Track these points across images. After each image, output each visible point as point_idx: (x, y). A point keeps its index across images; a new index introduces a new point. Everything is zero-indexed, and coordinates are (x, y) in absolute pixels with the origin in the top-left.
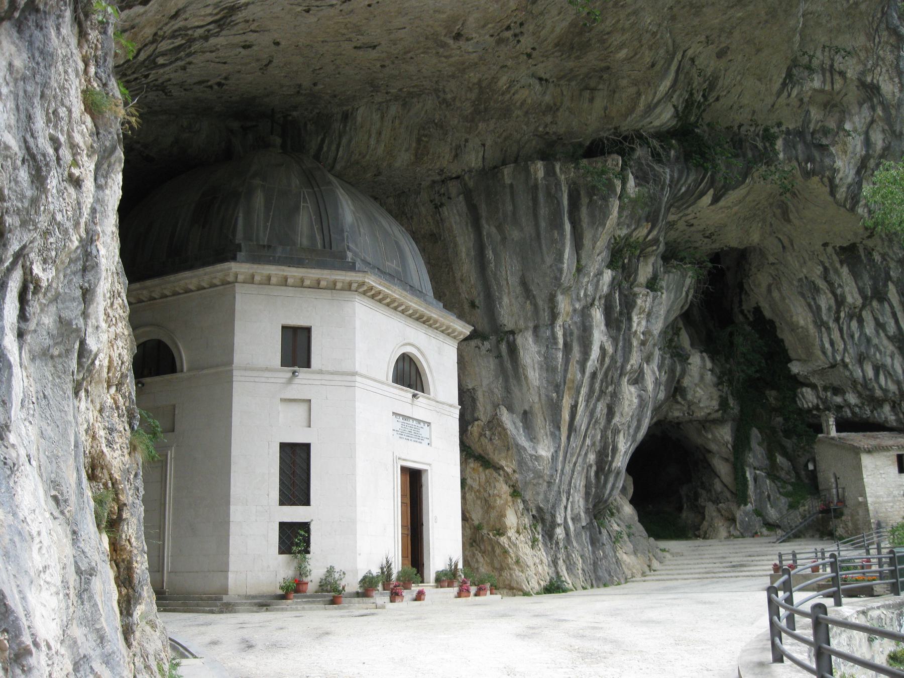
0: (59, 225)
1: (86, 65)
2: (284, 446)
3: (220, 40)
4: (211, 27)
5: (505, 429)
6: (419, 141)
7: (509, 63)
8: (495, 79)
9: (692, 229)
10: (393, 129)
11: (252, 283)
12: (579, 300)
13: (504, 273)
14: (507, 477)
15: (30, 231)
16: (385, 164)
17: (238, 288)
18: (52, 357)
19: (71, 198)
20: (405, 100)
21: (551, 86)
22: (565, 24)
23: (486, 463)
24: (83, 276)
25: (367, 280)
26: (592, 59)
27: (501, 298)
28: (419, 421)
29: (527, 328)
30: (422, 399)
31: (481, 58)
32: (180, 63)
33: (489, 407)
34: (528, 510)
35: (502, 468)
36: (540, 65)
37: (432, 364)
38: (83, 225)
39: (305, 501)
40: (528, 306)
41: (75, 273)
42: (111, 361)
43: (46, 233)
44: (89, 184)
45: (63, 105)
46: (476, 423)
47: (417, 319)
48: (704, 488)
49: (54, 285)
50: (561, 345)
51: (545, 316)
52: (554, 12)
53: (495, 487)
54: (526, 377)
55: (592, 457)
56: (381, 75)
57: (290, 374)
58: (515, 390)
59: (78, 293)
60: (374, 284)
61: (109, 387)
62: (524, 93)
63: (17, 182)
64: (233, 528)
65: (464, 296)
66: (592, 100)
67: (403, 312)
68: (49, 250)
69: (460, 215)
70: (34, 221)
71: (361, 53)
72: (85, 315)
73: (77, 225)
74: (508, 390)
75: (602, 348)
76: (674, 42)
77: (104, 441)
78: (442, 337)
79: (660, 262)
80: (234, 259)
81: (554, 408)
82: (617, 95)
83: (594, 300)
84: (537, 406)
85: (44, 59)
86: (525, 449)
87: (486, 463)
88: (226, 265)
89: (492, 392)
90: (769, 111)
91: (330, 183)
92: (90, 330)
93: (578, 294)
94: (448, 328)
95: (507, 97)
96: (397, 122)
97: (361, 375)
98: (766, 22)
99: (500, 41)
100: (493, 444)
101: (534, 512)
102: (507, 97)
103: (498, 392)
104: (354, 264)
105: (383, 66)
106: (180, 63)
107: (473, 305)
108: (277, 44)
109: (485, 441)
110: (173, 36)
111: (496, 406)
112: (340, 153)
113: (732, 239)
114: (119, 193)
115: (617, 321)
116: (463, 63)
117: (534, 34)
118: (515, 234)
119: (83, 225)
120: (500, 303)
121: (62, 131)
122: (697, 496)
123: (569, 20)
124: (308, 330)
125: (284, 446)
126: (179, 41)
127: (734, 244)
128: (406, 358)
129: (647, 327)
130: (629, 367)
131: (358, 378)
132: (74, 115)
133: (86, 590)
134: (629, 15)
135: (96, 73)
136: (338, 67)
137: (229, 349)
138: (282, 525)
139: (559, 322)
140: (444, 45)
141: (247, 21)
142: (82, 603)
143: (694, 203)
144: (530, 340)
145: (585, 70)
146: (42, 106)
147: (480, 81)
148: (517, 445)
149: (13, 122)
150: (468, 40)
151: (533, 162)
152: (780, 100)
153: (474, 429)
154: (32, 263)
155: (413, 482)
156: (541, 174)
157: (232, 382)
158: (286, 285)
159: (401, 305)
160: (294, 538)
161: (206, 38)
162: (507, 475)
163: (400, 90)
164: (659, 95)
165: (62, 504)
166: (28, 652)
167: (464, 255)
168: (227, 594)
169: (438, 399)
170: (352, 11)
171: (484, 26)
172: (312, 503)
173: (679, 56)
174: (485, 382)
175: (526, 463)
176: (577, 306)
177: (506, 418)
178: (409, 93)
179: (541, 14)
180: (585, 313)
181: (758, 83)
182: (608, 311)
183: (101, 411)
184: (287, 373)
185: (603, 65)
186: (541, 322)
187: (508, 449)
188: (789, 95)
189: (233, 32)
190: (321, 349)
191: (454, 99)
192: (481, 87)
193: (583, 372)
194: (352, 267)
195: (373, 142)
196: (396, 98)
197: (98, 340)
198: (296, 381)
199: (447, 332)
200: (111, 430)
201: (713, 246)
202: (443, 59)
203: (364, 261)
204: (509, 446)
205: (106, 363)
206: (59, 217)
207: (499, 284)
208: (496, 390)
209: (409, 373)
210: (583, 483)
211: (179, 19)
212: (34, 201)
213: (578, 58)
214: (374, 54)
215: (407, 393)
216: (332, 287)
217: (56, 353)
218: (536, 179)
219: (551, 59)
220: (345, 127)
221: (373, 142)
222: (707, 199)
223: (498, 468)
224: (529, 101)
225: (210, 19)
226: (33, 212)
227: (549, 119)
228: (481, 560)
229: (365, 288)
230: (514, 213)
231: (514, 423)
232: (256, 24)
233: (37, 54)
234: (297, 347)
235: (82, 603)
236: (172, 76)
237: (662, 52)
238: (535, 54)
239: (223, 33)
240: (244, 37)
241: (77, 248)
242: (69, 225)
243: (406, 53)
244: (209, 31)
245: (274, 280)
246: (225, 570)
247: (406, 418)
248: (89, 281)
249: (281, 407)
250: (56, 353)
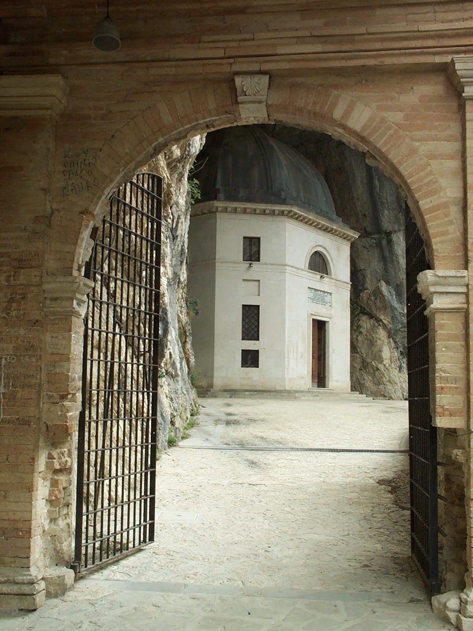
2: (244, 307)
5: (384, 296)
11: (226, 212)
13: (385, 194)
17: (218, 215)
24: (181, 257)
25: (293, 210)
28: (324, 292)
29: (400, 230)
30: (326, 279)
34: (397, 348)
35: (381, 320)
46: (365, 291)
47: (324, 230)
53: (376, 333)
59: (180, 263)
60: (297, 212)
65: (359, 208)
67: (315, 226)
78: (340, 240)
80: (216, 198)
88: (211, 202)
91: (272, 147)
94: (344, 234)
97: (289, 266)
100: (375, 305)
104: (285, 199)
109: (371, 303)
124: (259, 239)
125: (244, 307)
128: (317, 253)
131: (287, 267)
137: (213, 251)
148: (391, 306)
153: (364, 295)
155: (320, 327)
157: (215, 269)
158: (246, 213)
159: (313, 223)
160: (250, 359)
162: (384, 325)
168: (213, 388)
169: (460, 195)
175: (397, 318)
177: (384, 287)
187: (386, 309)
194: (284, 202)
198: (252, 269)
199: (345, 237)
215: (318, 276)
216: (273, 213)
223: (379, 320)
228: (366, 378)
229: (292, 214)
231: (390, 292)
234: (252, 250)
247: (316, 290)
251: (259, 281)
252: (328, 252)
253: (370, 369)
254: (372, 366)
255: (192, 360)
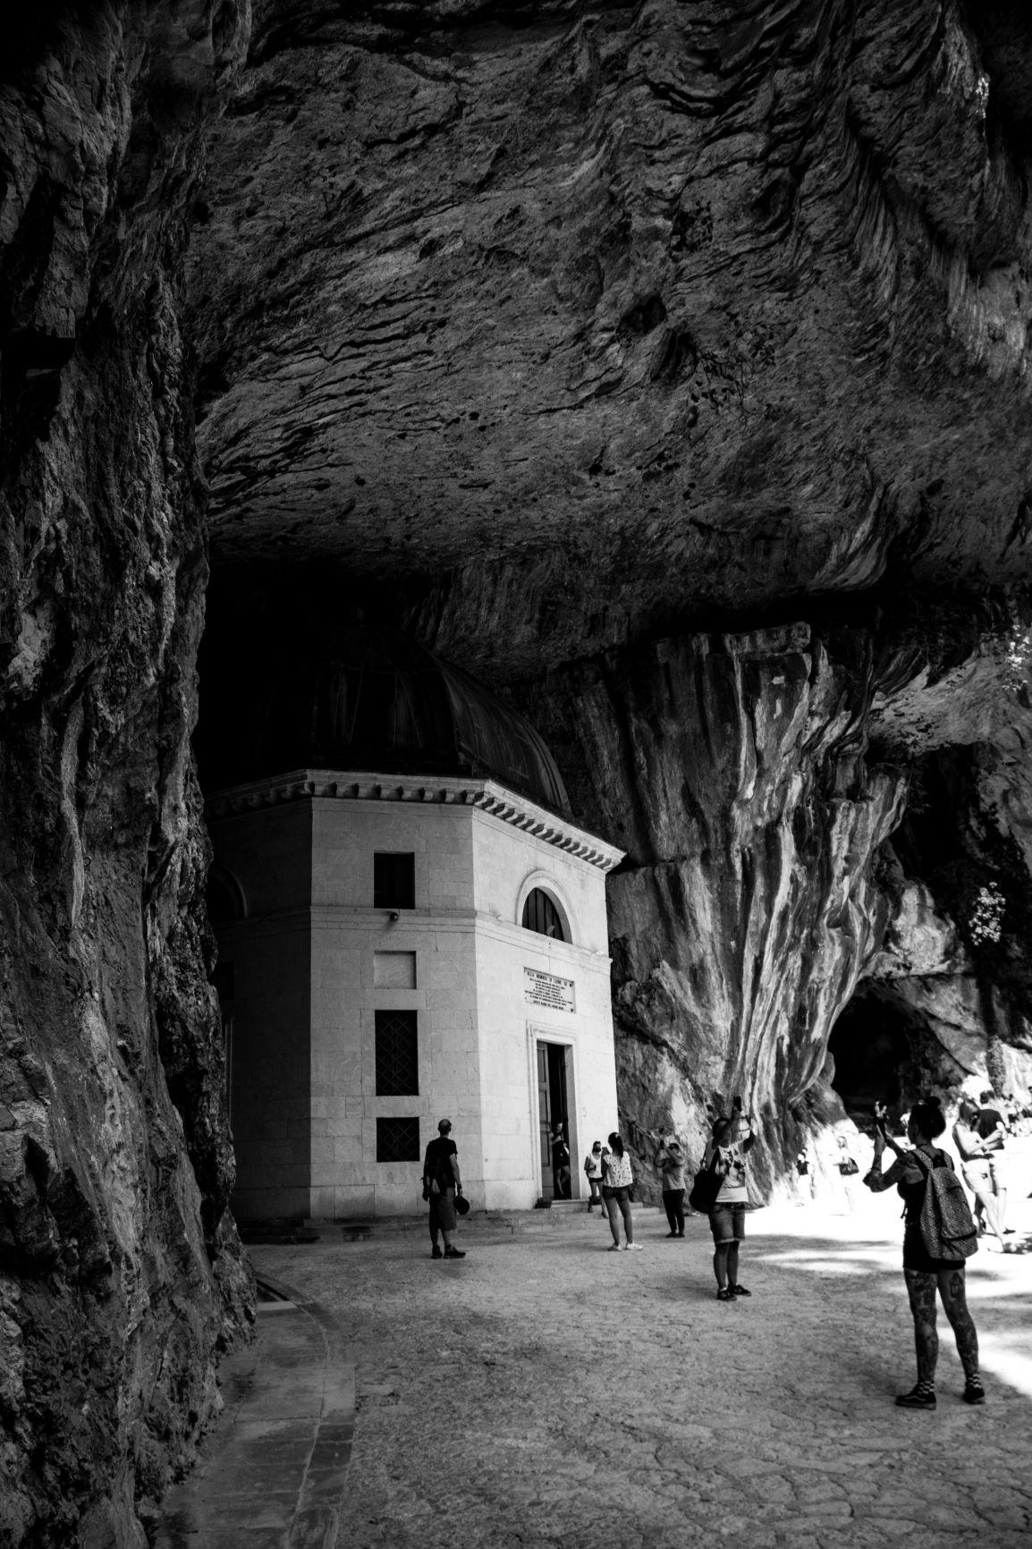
0: (133, 648)
1: (163, 433)
3: (288, 478)
4: (278, 457)
6: (543, 610)
7: (661, 505)
8: (642, 526)
9: (904, 720)
10: (510, 595)
12: (761, 815)
14: (673, 1055)
15: (99, 644)
16: (500, 641)
18: (116, 847)
19: (146, 610)
20: (526, 556)
21: (715, 535)
22: (732, 452)
23: (648, 1038)
26: (767, 498)
27: (657, 816)
29: (693, 855)
31: (624, 498)
32: (234, 510)
33: (645, 963)
35: (665, 1044)
36: (702, 507)
37: (574, 902)
38: (161, 654)
39: (411, 1088)
40: (694, 825)
41: (148, 725)
42: (184, 867)
43: (116, 658)
44: (170, 596)
45: (140, 476)
48: (927, 1066)
49: (122, 739)
50: (739, 877)
51: (716, 839)
52: (718, 435)
54: (694, 921)
55: (784, 1028)
56: (494, 525)
57: (385, 919)
58: (681, 939)
59: (153, 754)
61: (180, 906)
62: (679, 546)
63: (88, 564)
64: (315, 1127)
66: (768, 552)
67: (534, 832)
68: (119, 684)
69: (599, 707)
70: (104, 630)
71: (468, 493)
72: (162, 789)
73: (155, 651)
74: (670, 939)
75: (793, 879)
76: (872, 473)
77: (174, 981)
79: (863, 765)
81: (734, 964)
82: (800, 545)
83: (780, 815)
84: (709, 959)
85: (120, 401)
86: (695, 1017)
87: (648, 1038)
89: (650, 942)
90: (998, 562)
92: (166, 811)
93: (760, 808)
95: (659, 548)
96: (514, 587)
98: (991, 445)
99: (648, 477)
100: (651, 1011)
101: (709, 1102)
102: (659, 548)
103: (657, 942)
105: (497, 511)
106: (234, 510)
107: (621, 827)
108: (360, 482)
109: (639, 1007)
110: (231, 469)
111: (655, 964)
112: (441, 629)
113: (954, 730)
114: (202, 624)
115: (813, 846)
116: (601, 506)
117: (692, 466)
118: (672, 729)
119: (161, 654)
120: (657, 822)
121: (139, 512)
122: (918, 1078)
123: (737, 447)
124: (409, 858)
126: (238, 477)
127: (957, 739)
129: (850, 850)
130: (828, 905)
132: (153, 494)
133: (163, 1189)
134: (814, 439)
135: (176, 448)
136: (438, 514)
138: (381, 1121)
139: (736, 845)
140: (577, 482)
141: (323, 451)
142: (160, 1207)
143: (904, 685)
144: (698, 870)
145: (757, 513)
146: (116, 470)
147: (623, 529)
148: (685, 1012)
149: (82, 478)
150: (608, 473)
151: (695, 634)
152: (1011, 547)
154: (96, 699)
155: (555, 1059)
156: (705, 650)
161: (271, 473)
162: (671, 1051)
163: (519, 543)
164: (855, 544)
165: (132, 1059)
166: (107, 1270)
167: (606, 759)
170: (460, 437)
171: (629, 455)
172: (421, 1091)
173: (879, 492)
174: (639, 928)
175: (697, 1037)
176: (760, 823)
178: (530, 548)
179: (701, 438)
180: (769, 836)
181: (983, 526)
182: (799, 829)
183: (170, 939)
184: (380, 918)
185: (782, 505)
186: (712, 846)
187: (672, 1018)
188: (1023, 540)
189: (305, 466)
190: (430, 884)
191: (589, 554)
192: (623, 537)
193: (769, 912)
194: (465, 773)
195: (483, 612)
196: (514, 554)
197: (176, 829)
198: (397, 926)
199: (592, 858)
200: (183, 966)
201: (930, 743)
202: (576, 501)
203: (481, 764)
204: (674, 1014)
205: (178, 868)
206: (132, 637)
207: (655, 800)
208: (654, 940)
209: (543, 915)
210: (773, 1061)
211: (241, 444)
212: (108, 599)
213: (749, 497)
214: (484, 496)
216: (441, 798)
217: (121, 840)
218: (700, 656)
219: (715, 500)
220: (447, 593)
221: (483, 612)
222: (921, 679)
223: (660, 1044)
224: (687, 554)
225: (277, 446)
226: (104, 616)
227: (712, 577)
229: (484, 800)
230: (672, 700)
232: (335, 455)
233: (111, 393)
234: (395, 883)
235: (160, 1207)
236: (224, 528)
237: (858, 487)
238: (693, 493)
239: (293, 467)
240: (319, 474)
241: (153, 686)
242: (145, 648)
243: (527, 493)
244: (275, 462)
245: (363, 792)
246: (306, 1185)
248: (167, 738)
249: (376, 962)
250: (121, 840)
251: (413, 953)
252: (561, 888)
253: (647, 1145)
254: (651, 1141)
255: (228, 1162)
